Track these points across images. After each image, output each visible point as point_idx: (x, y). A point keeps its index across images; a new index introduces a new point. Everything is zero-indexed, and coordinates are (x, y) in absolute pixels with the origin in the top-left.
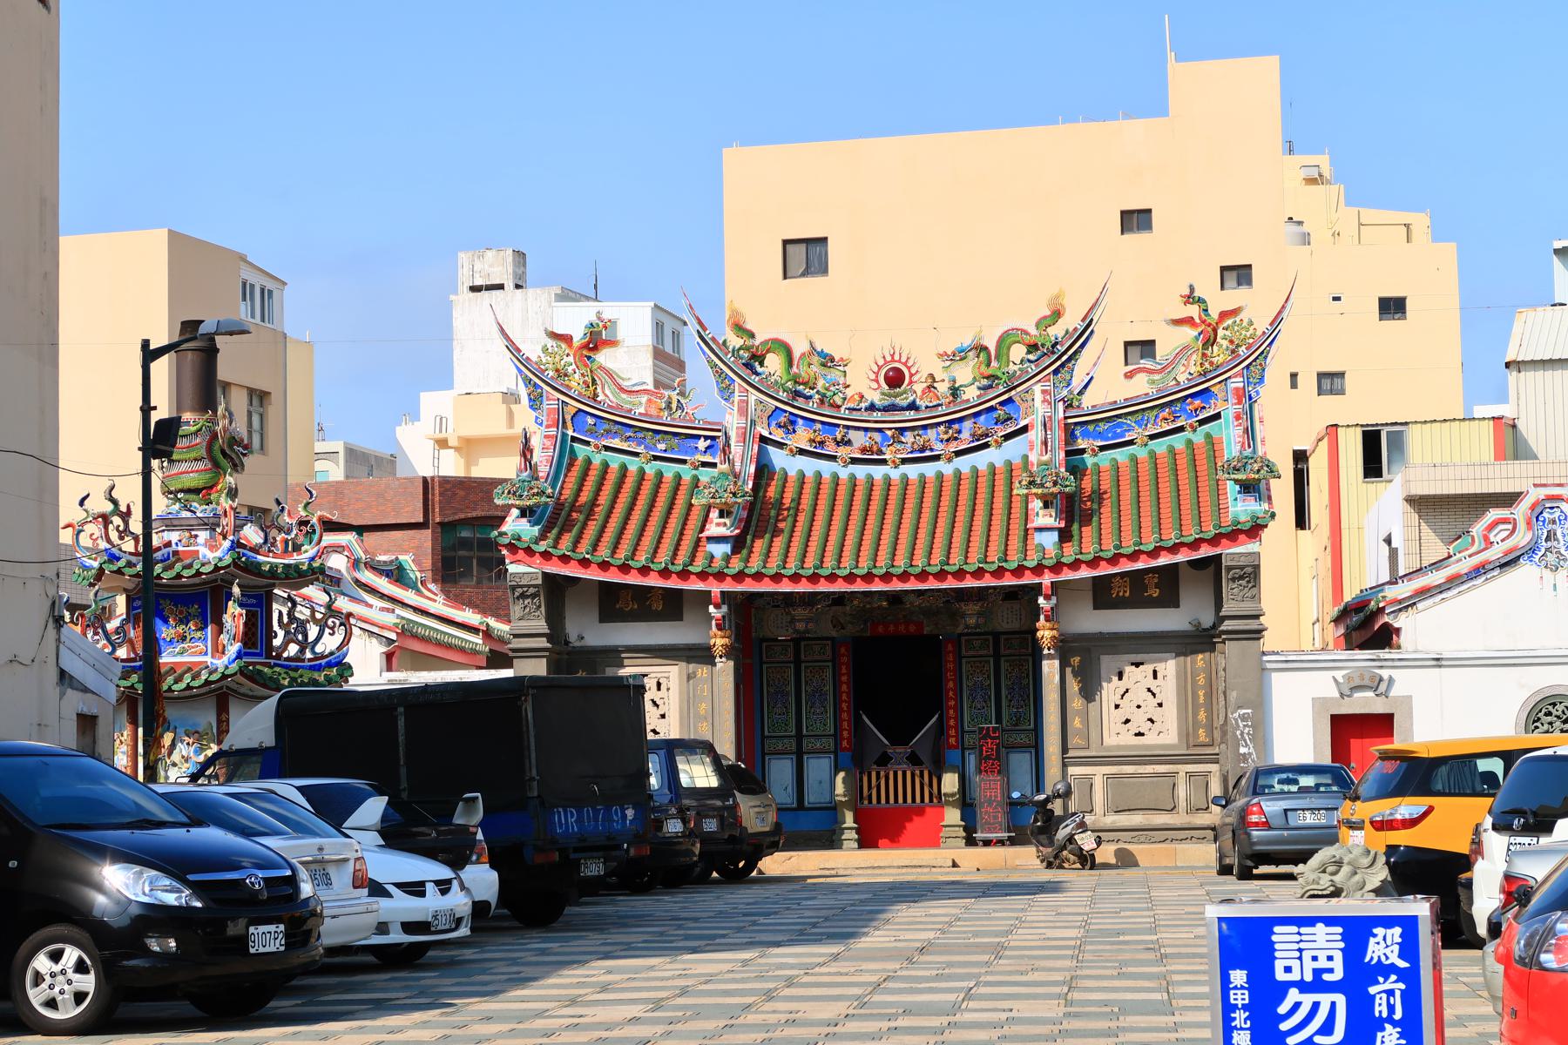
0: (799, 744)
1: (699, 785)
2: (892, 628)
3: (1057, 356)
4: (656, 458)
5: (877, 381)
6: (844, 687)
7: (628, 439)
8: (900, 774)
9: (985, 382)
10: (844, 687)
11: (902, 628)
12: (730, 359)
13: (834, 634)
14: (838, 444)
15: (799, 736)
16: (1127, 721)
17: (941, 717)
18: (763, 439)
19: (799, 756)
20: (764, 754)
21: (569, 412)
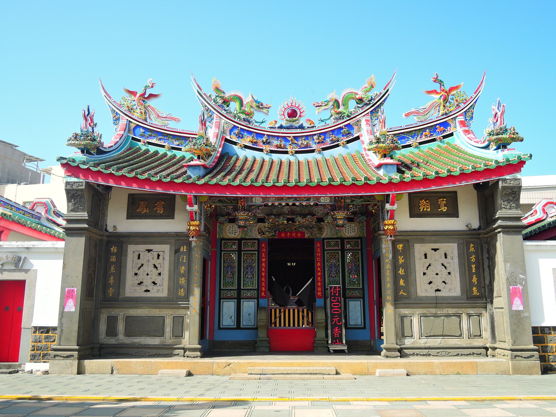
1: (158, 310)
2: (289, 234)
3: (373, 106)
4: (173, 148)
5: (284, 115)
6: (263, 264)
7: (160, 139)
8: (291, 311)
9: (337, 116)
10: (263, 264)
11: (294, 235)
12: (212, 103)
13: (259, 237)
14: (264, 143)
15: (239, 290)
16: (430, 283)
17: (313, 280)
18: (226, 140)
19: (239, 300)
21: (133, 126)
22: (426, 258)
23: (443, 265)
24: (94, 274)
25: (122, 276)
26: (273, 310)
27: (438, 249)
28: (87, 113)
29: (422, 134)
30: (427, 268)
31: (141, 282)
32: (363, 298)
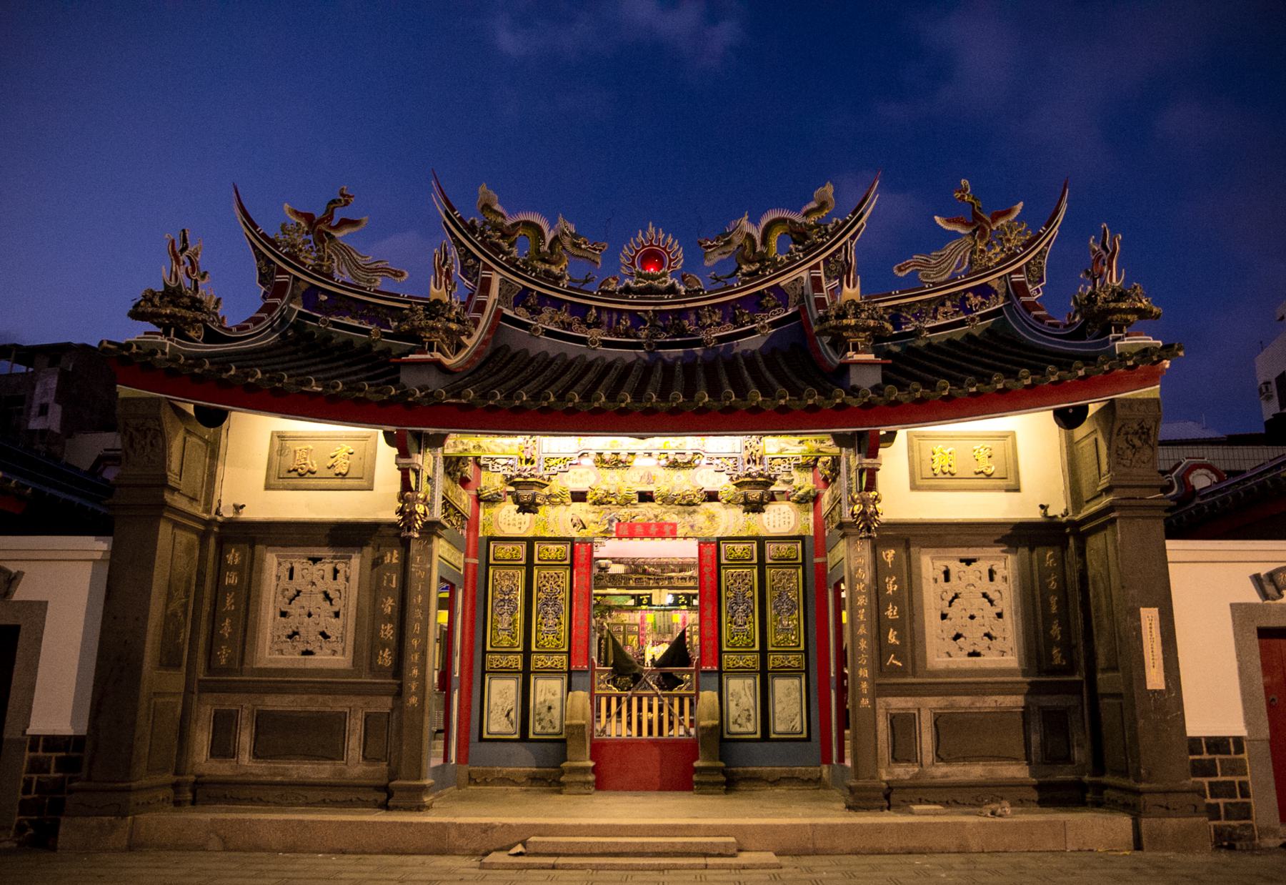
0: (527, 662)
15: (527, 653)
16: (957, 637)
20: (484, 672)
22: (947, 579)
23: (985, 595)
24: (185, 613)
25: (251, 616)
26: (604, 701)
27: (974, 560)
28: (178, 247)
29: (936, 310)
30: (951, 602)
31: (295, 633)
32: (807, 672)
